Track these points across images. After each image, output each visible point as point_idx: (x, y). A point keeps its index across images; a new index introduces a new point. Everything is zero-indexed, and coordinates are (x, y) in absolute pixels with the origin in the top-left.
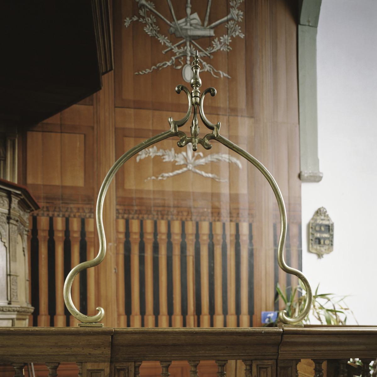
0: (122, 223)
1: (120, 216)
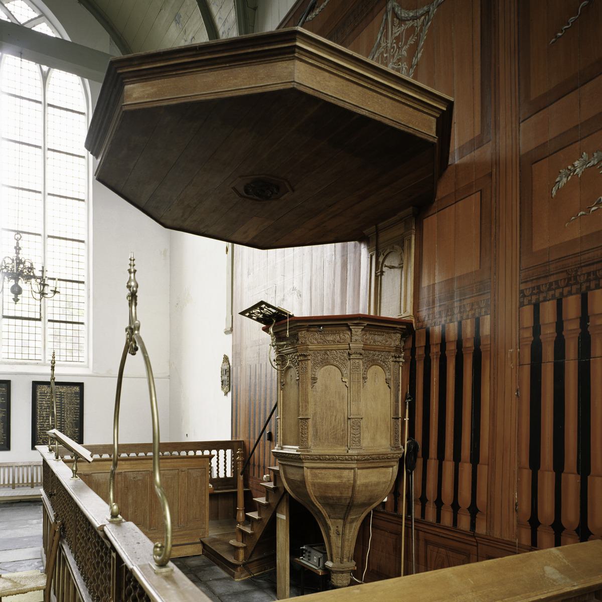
0: (528, 311)
1: (526, 302)
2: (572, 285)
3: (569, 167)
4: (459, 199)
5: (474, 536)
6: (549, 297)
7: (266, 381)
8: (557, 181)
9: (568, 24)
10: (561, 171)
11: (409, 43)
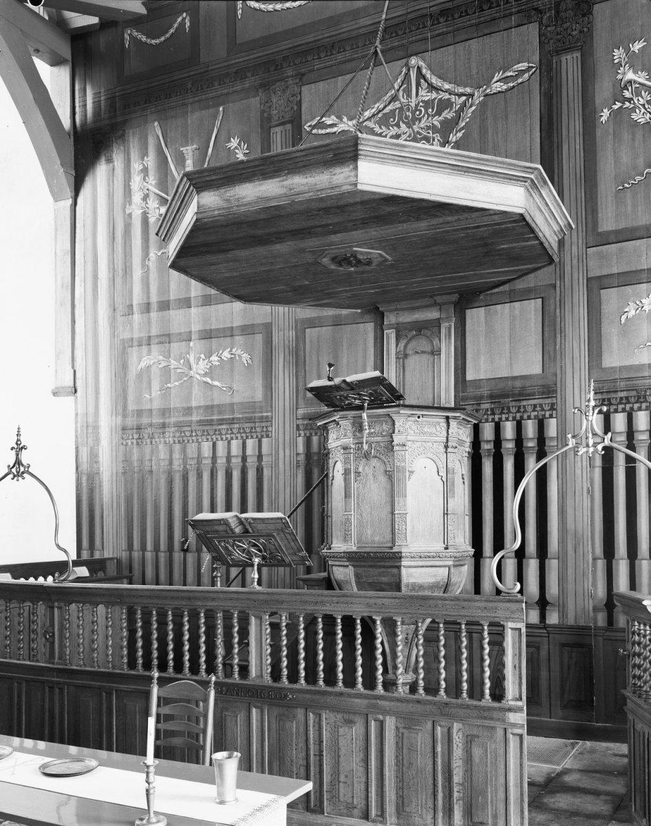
2: (641, 402)
3: (638, 302)
4: (516, 299)
5: (545, 628)
6: (620, 410)
7: (244, 458)
8: (625, 310)
9: (635, 181)
10: (630, 303)
11: (444, 114)
